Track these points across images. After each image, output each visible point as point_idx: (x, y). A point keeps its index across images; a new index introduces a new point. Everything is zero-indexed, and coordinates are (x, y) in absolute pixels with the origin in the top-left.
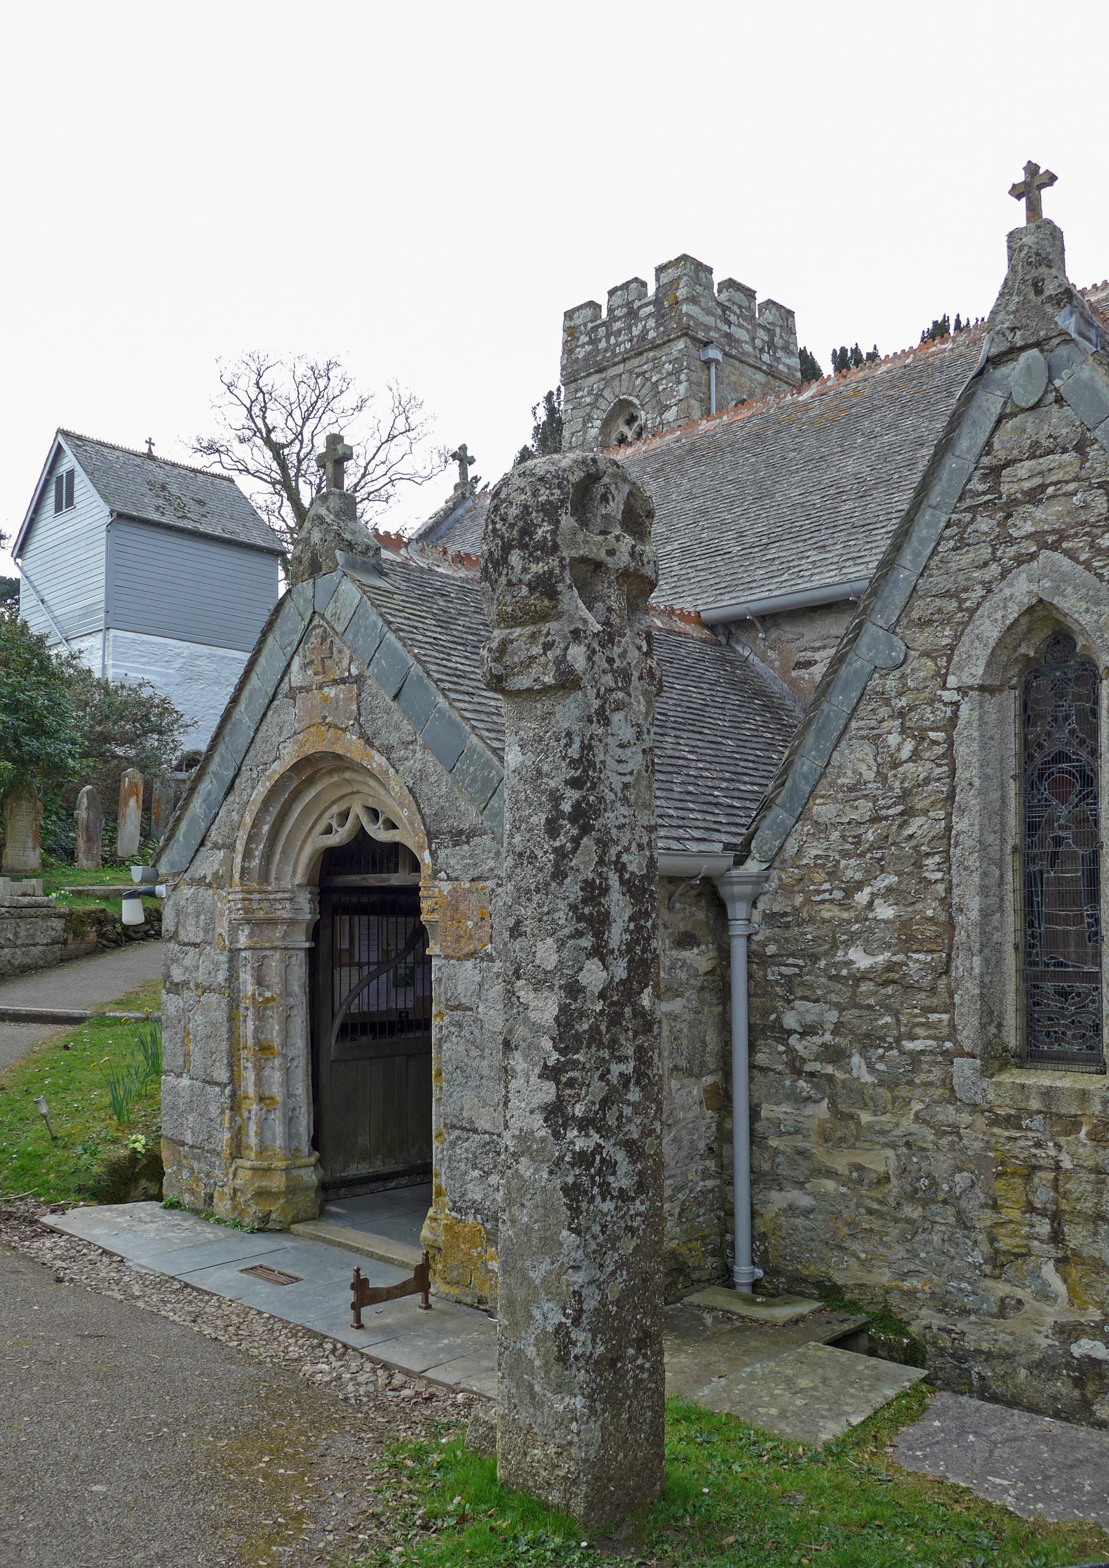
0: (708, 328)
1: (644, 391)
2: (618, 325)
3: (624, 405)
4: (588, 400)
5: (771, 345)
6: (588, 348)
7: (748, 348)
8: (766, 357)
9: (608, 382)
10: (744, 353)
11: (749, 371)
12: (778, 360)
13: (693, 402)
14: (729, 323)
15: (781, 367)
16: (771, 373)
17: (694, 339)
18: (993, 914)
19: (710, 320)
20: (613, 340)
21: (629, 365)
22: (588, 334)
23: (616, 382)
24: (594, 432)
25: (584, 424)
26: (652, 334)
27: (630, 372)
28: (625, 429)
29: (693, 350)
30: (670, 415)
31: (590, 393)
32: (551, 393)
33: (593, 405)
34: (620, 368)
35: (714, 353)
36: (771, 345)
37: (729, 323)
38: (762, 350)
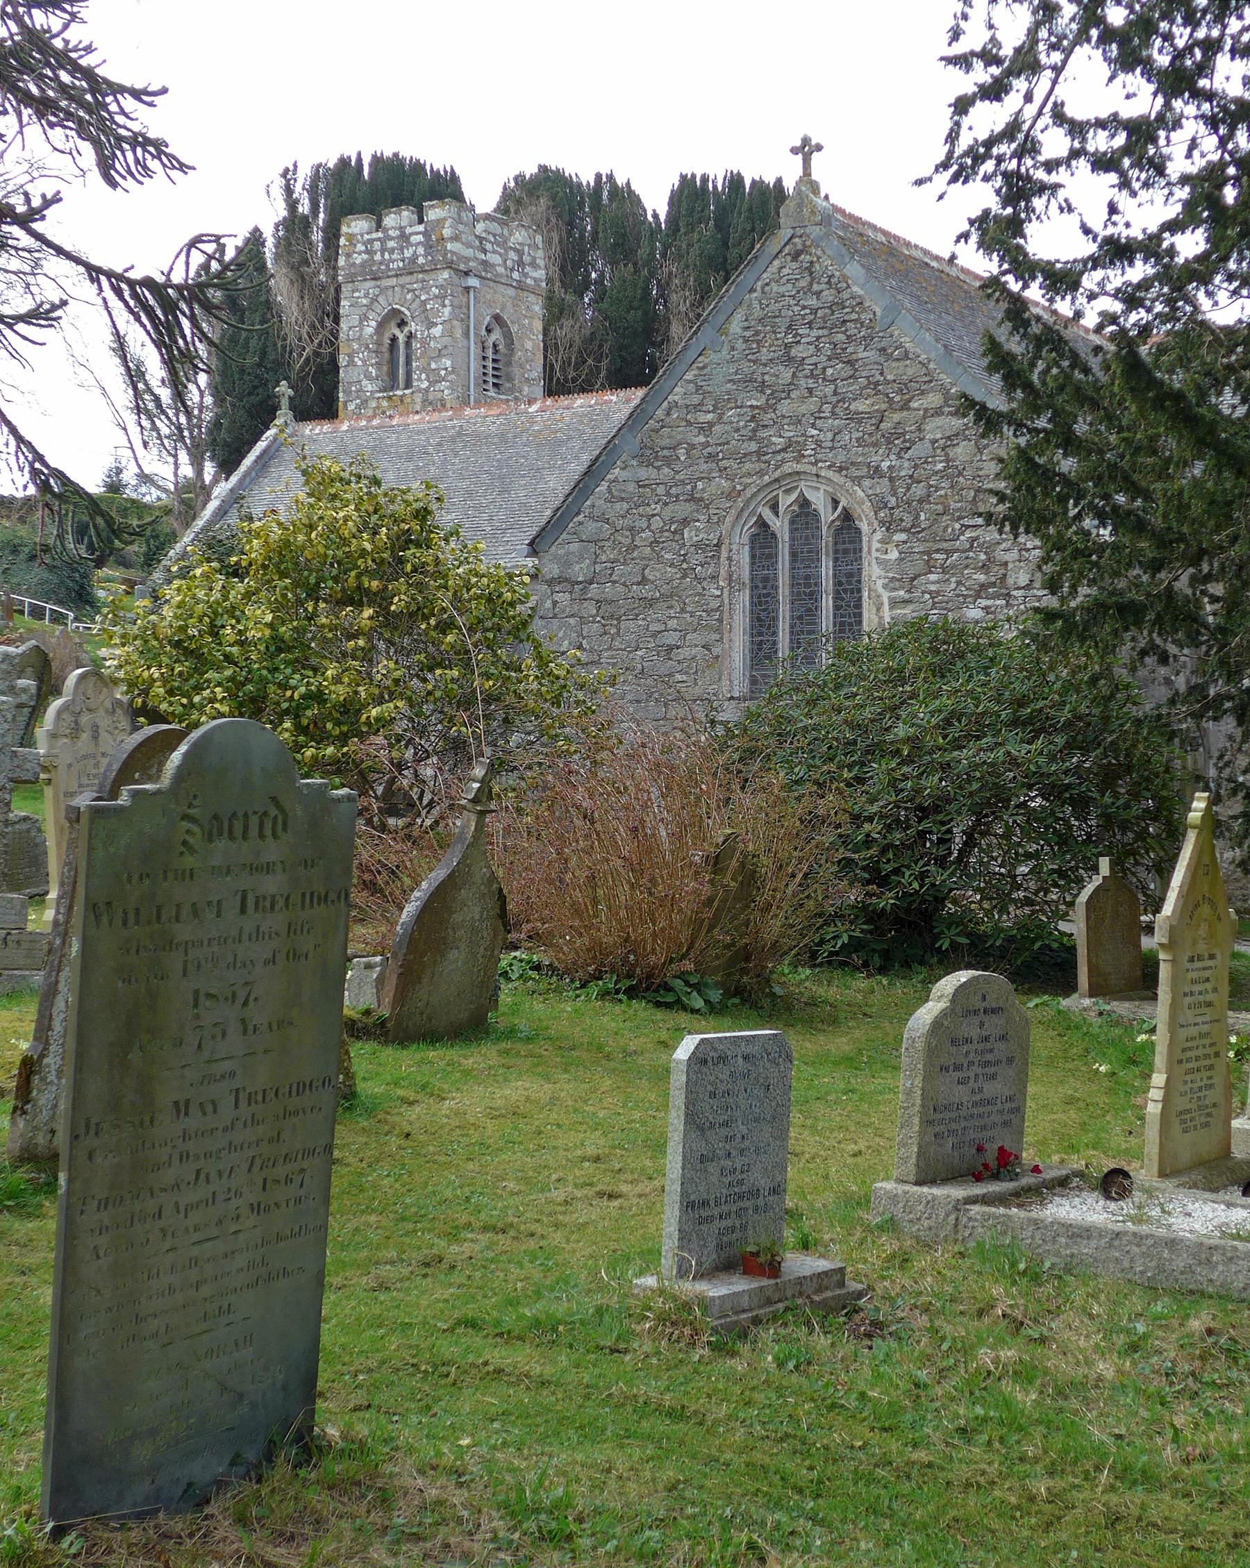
0: (468, 259)
1: (414, 306)
2: (391, 244)
3: (395, 312)
4: (364, 301)
5: (520, 263)
6: (365, 256)
7: (501, 270)
8: (516, 275)
9: (383, 290)
10: (497, 275)
11: (501, 288)
12: (526, 275)
13: (455, 322)
14: (485, 251)
15: (529, 281)
16: (521, 287)
17: (457, 271)
18: (186, 649)
19: (469, 252)
20: (387, 256)
21: (402, 280)
22: (364, 244)
23: (390, 292)
24: (370, 330)
25: (361, 322)
26: (421, 260)
27: (402, 286)
28: (397, 332)
29: (456, 279)
30: (437, 331)
31: (366, 296)
32: (287, 170)
33: (369, 307)
34: (393, 281)
35: (473, 282)
36: (520, 263)
37: (485, 251)
38: (512, 270)
